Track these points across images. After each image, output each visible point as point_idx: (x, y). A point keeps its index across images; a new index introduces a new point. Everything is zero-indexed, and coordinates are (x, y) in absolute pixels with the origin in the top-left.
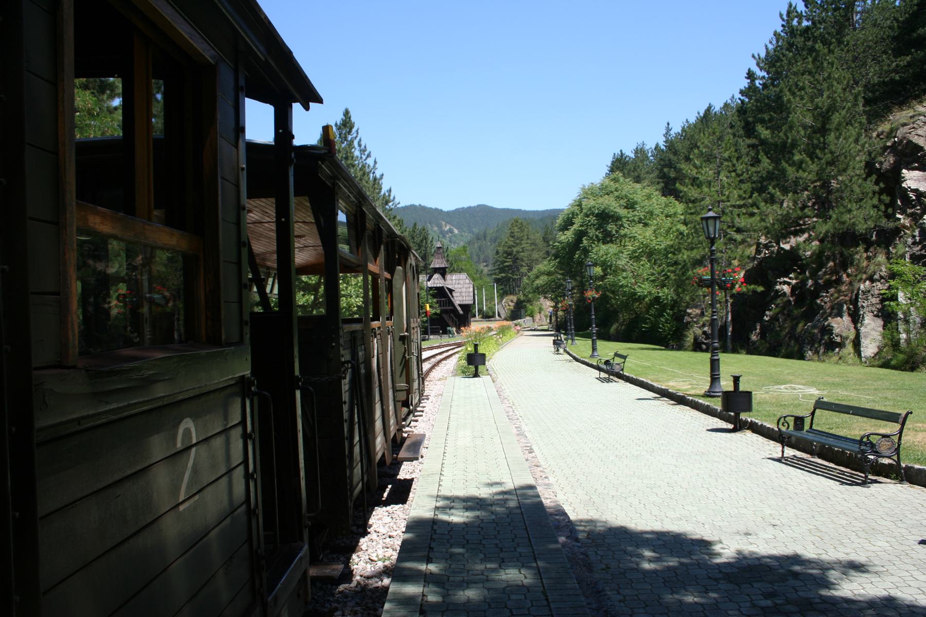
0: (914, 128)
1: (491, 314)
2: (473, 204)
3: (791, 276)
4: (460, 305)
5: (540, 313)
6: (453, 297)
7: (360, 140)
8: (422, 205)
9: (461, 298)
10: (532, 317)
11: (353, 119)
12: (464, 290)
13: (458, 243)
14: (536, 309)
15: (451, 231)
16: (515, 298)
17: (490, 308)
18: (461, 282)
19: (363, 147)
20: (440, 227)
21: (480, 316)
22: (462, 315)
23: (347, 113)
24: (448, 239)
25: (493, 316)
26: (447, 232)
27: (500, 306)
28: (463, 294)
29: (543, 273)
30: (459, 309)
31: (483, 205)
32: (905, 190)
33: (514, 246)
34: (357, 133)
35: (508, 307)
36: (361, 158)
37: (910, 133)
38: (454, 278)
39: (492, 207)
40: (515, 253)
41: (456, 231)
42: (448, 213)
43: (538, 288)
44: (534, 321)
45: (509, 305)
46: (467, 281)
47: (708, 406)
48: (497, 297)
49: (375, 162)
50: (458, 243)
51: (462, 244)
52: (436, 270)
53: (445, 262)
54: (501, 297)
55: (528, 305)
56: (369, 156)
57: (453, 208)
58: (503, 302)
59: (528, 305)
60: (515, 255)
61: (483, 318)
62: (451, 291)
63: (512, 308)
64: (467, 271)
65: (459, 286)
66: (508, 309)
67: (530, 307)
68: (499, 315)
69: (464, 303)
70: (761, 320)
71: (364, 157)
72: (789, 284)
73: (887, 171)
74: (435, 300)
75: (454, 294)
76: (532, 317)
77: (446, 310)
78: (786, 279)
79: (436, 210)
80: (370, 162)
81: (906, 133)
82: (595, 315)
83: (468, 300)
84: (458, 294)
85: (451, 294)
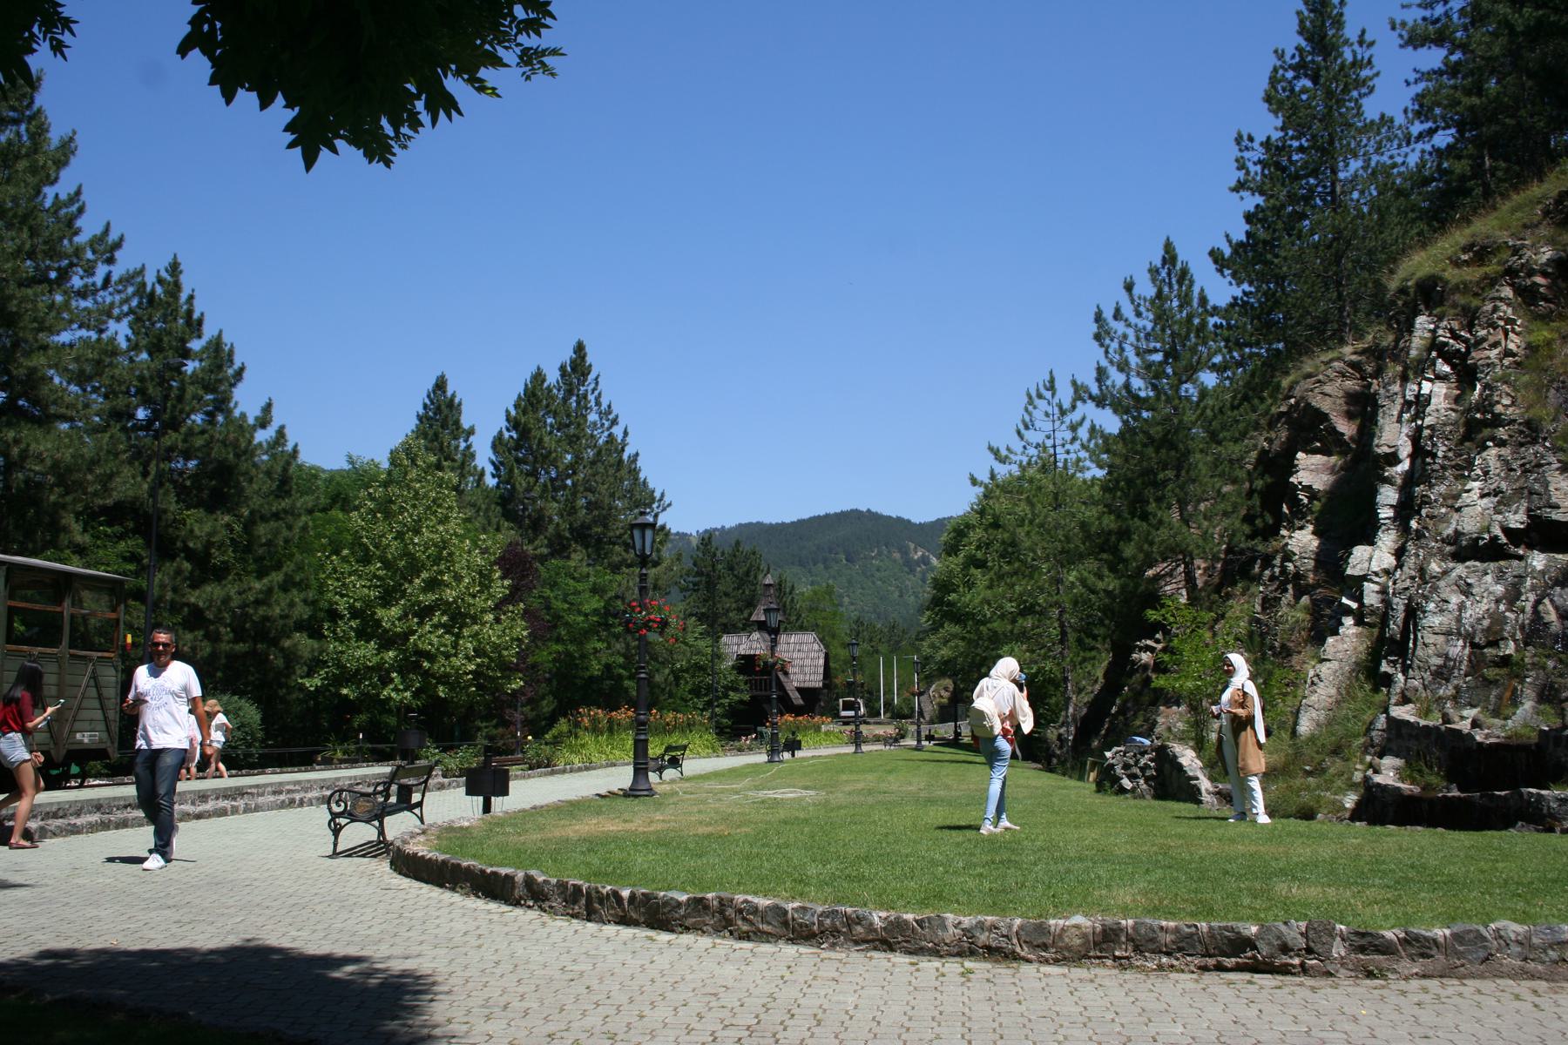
0: (1319, 381)
1: (906, 711)
3: (1157, 636)
4: (799, 690)
7: (600, 394)
8: (873, 510)
9: (801, 677)
11: (589, 360)
12: (808, 662)
15: (925, 560)
18: (805, 648)
19: (604, 406)
20: (905, 552)
21: (888, 715)
23: (580, 349)
24: (919, 575)
26: (918, 563)
28: (807, 669)
32: (1294, 488)
34: (597, 383)
36: (603, 425)
37: (1312, 390)
45: (941, 697)
46: (816, 647)
49: (626, 433)
56: (614, 422)
57: (933, 519)
61: (892, 718)
63: (945, 701)
64: (814, 628)
65: (801, 655)
69: (807, 685)
70: (1108, 714)
71: (607, 424)
72: (1152, 650)
73: (1278, 454)
78: (1149, 642)
79: (899, 520)
80: (617, 431)
81: (1307, 390)
83: (815, 680)
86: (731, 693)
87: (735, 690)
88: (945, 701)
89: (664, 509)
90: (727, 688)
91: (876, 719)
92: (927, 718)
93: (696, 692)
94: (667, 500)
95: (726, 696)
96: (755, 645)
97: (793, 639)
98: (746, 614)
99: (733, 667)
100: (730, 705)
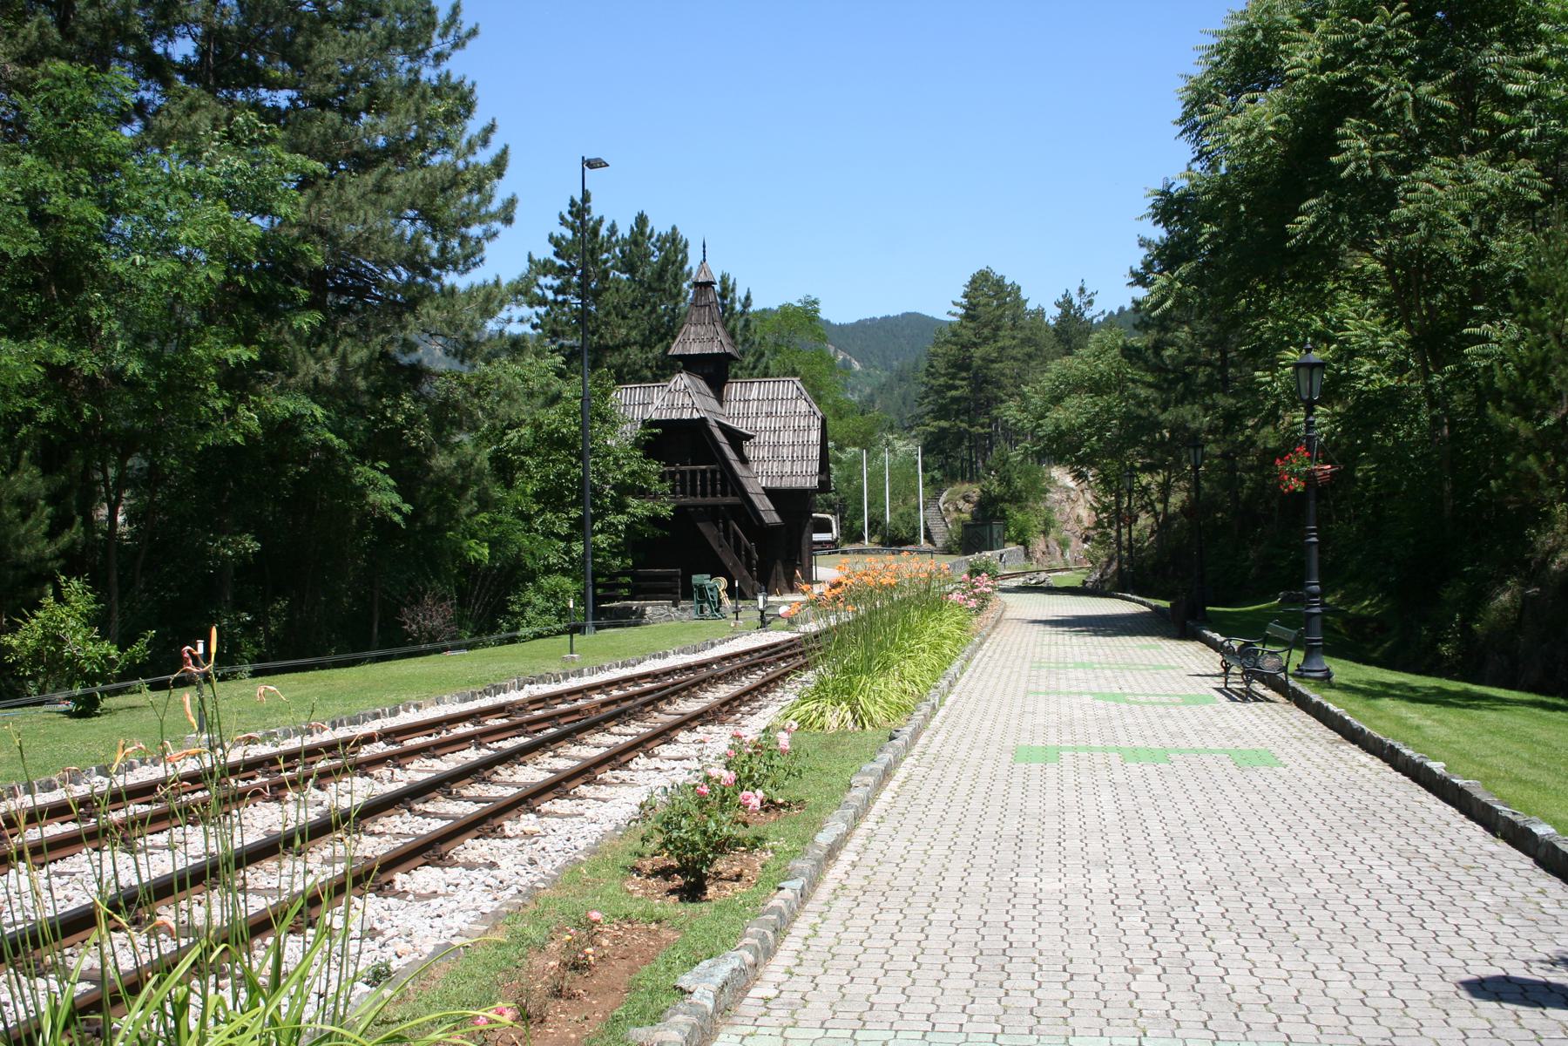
1: (904, 533)
2: (895, 310)
4: (770, 492)
5: (1045, 533)
6: (744, 461)
10: (1025, 543)
12: (787, 437)
13: (860, 391)
14: (1036, 522)
16: (974, 491)
17: (901, 516)
18: (781, 408)
21: (876, 539)
22: (773, 528)
25: (912, 540)
27: (933, 510)
28: (785, 452)
29: (1076, 387)
30: (764, 505)
31: (915, 314)
33: (975, 345)
35: (955, 515)
38: (754, 395)
39: (933, 318)
40: (977, 362)
41: (857, 366)
42: (842, 328)
43: (1059, 435)
44: (1027, 555)
45: (958, 510)
46: (803, 406)
47: (1319, 704)
48: (925, 485)
50: (860, 391)
51: (868, 390)
52: (692, 364)
53: (722, 336)
54: (935, 486)
55: (1011, 510)
57: (854, 320)
58: (942, 499)
59: (1011, 510)
60: (979, 368)
62: (737, 439)
63: (967, 517)
66: (956, 521)
67: (1019, 516)
68: (929, 537)
69: (786, 483)
74: (654, 466)
75: (749, 450)
76: (1025, 543)
77: (715, 507)
82: (1304, 548)
83: (804, 475)
84: (763, 453)
85: (739, 451)
86: (632, 502)
87: (642, 493)
88: (967, 517)
89: (459, 44)
90: (623, 489)
91: (857, 546)
92: (940, 543)
93: (551, 497)
94: (466, 22)
95: (620, 508)
96: (680, 399)
97: (755, 391)
98: (658, 350)
99: (637, 444)
100: (629, 527)
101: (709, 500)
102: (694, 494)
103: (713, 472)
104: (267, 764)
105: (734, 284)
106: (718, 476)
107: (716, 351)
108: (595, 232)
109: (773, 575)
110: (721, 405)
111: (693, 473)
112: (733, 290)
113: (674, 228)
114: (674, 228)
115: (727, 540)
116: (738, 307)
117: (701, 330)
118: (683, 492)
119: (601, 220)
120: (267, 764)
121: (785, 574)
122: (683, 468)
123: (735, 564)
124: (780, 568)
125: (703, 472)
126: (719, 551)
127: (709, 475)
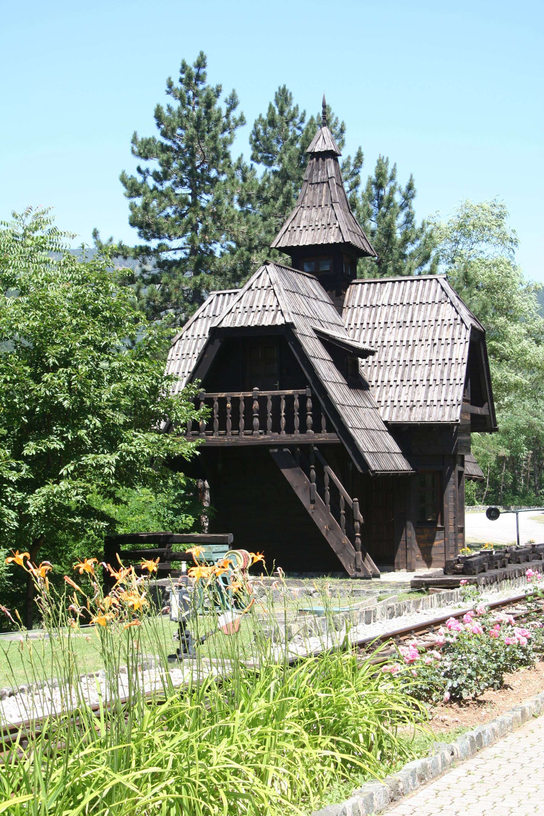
46: (447, 312)
77: (305, 447)
84: (390, 375)
101: (297, 437)
102: (276, 428)
103: (303, 399)
104: (413, 631)
105: (394, 170)
106: (309, 404)
107: (332, 240)
108: (209, 104)
109: (402, 543)
110: (340, 313)
111: (276, 400)
112: (392, 178)
113: (285, 86)
114: (285, 86)
115: (322, 494)
116: (398, 198)
117: (315, 214)
118: (263, 426)
119: (218, 91)
120: (413, 631)
121: (419, 541)
122: (263, 393)
123: (332, 528)
124: (410, 532)
125: (290, 399)
126: (310, 508)
127: (297, 403)
